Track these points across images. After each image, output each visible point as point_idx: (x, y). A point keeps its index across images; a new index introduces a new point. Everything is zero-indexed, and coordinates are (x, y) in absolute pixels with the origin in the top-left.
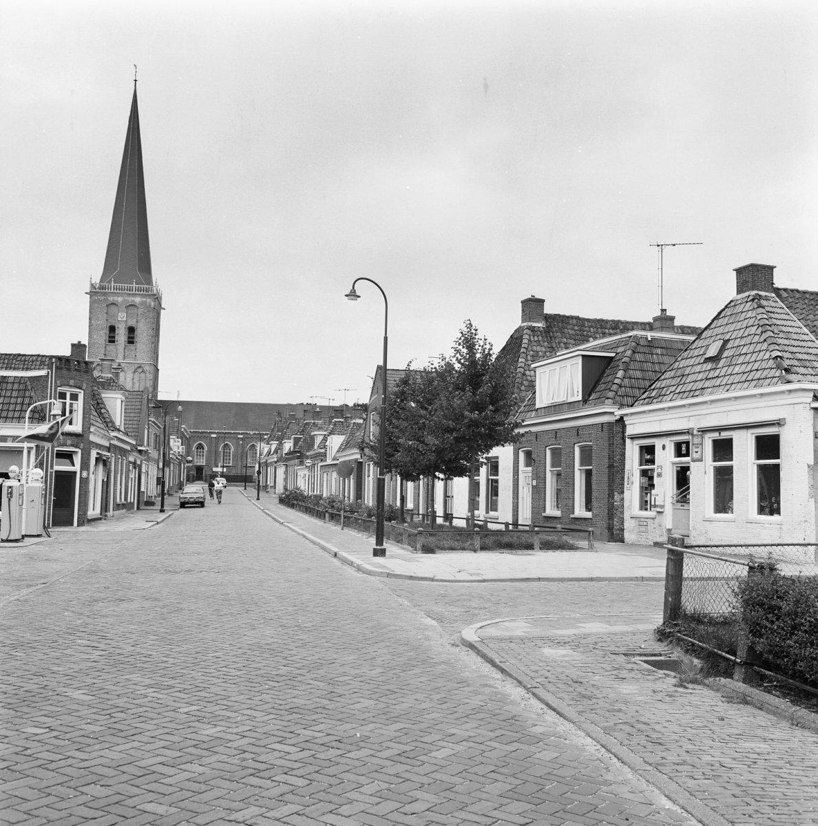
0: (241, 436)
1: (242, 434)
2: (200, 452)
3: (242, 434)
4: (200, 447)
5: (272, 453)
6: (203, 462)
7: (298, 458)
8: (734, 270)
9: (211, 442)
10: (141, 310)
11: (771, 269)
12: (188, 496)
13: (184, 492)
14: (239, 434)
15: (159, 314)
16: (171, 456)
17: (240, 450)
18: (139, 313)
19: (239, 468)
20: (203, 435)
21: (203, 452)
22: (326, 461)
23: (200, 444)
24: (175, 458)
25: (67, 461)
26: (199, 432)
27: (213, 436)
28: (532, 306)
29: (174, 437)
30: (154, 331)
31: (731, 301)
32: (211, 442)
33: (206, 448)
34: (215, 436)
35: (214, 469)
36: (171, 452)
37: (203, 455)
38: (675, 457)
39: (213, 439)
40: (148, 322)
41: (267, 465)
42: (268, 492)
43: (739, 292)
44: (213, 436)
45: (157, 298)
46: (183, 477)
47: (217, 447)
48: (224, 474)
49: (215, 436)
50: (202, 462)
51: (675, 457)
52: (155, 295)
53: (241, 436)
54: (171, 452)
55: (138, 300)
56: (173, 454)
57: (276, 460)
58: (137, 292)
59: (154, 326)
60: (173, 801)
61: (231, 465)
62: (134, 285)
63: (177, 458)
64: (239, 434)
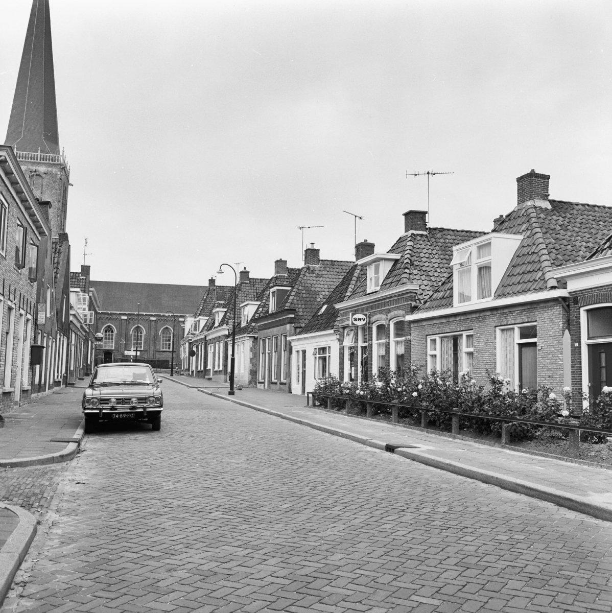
0: (154, 319)
1: (154, 316)
2: (109, 335)
3: (154, 316)
4: (109, 329)
5: (216, 325)
6: (112, 346)
7: (291, 321)
8: (403, 215)
9: (121, 325)
10: (46, 181)
11: (423, 214)
12: (105, 392)
13: (98, 381)
14: (152, 316)
15: (66, 191)
16: (71, 318)
17: (153, 333)
18: (44, 184)
19: (152, 352)
20: (112, 317)
21: (112, 335)
22: (450, 304)
23: (109, 326)
24: (79, 327)
25: (285, 378)
26: (108, 314)
27: (123, 317)
28: (245, 274)
29: (78, 290)
30: (61, 204)
31: (400, 238)
32: (121, 325)
33: (115, 332)
34: (125, 317)
35: (126, 353)
36: (72, 312)
37: (112, 339)
38: (394, 338)
39: (123, 321)
40: (54, 194)
41: (206, 342)
42: (210, 379)
43: (406, 231)
44: (123, 317)
45: (64, 168)
46: (91, 359)
47: (127, 330)
48: (138, 358)
49: (125, 317)
50: (110, 346)
51: (394, 338)
52: (61, 165)
53: (154, 319)
54: (72, 312)
55: (42, 169)
56: (74, 315)
57: (226, 332)
58: (42, 161)
59: (61, 198)
60: (97, 554)
61: (142, 349)
62: (39, 154)
63: (82, 327)
64: (152, 316)
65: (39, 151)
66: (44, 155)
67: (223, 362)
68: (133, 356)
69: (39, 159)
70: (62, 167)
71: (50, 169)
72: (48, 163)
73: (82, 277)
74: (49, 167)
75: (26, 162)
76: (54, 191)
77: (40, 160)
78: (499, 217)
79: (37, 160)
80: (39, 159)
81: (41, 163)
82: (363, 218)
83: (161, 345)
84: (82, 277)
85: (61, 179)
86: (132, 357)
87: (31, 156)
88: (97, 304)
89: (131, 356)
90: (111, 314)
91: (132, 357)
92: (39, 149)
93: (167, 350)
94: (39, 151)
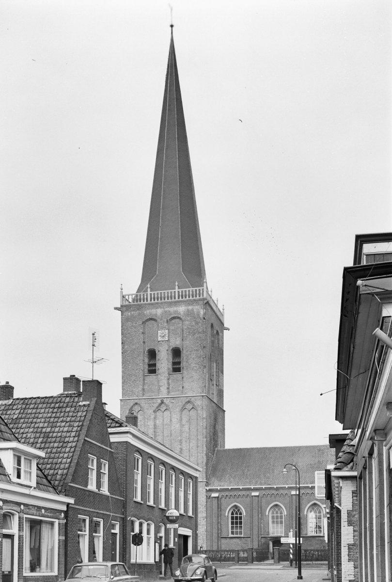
52: (204, 299)
55: (182, 309)
65: (177, 287)
66: (182, 291)
67: (170, 540)
68: (293, 544)
69: (149, 299)
70: (205, 301)
71: (190, 308)
72: (188, 300)
73: (84, 403)
74: (189, 304)
75: (162, 303)
76: (197, 335)
77: (179, 298)
78: (224, 409)
79: (175, 299)
80: (149, 299)
81: (152, 304)
82: (170, 24)
83: (230, 523)
84: (84, 403)
85: (204, 319)
86: (291, 546)
87: (161, 296)
88: (134, 435)
89: (290, 544)
90: (277, 489)
91: (291, 546)
92: (177, 284)
93: (239, 536)
94: (149, 290)
